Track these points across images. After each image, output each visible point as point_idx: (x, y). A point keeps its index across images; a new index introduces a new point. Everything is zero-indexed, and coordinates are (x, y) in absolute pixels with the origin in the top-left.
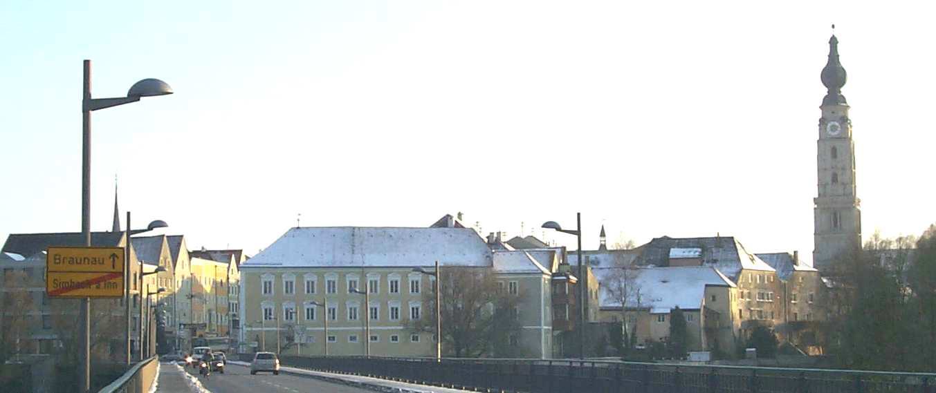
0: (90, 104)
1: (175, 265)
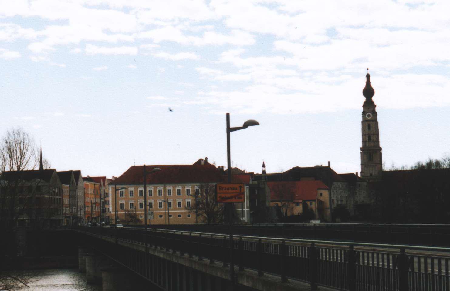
0: (230, 130)
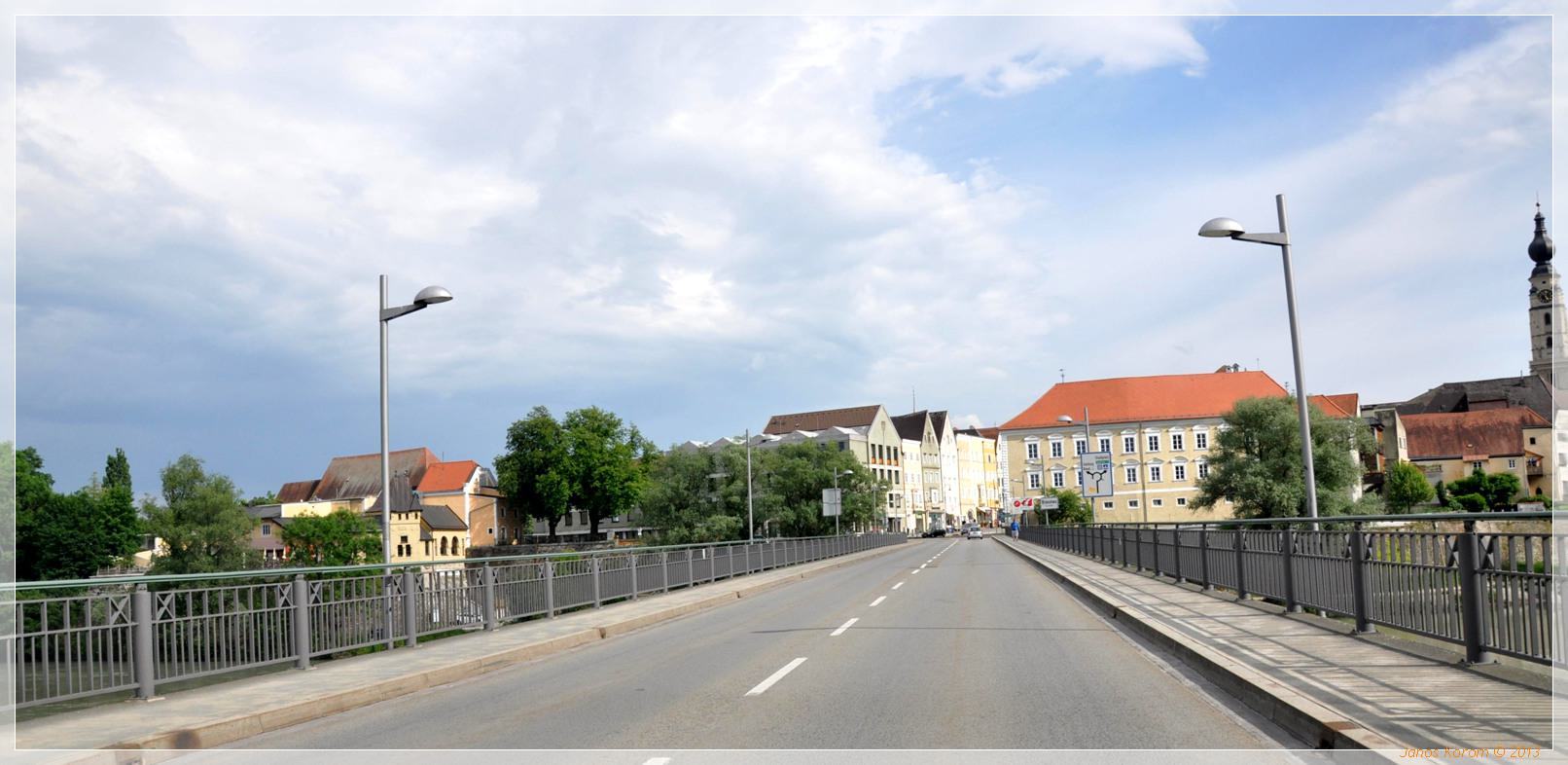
1: (939, 441)
